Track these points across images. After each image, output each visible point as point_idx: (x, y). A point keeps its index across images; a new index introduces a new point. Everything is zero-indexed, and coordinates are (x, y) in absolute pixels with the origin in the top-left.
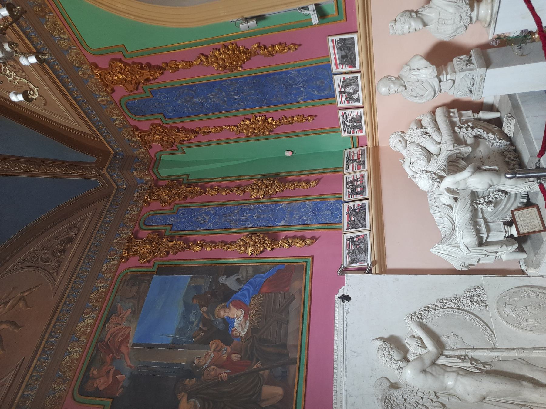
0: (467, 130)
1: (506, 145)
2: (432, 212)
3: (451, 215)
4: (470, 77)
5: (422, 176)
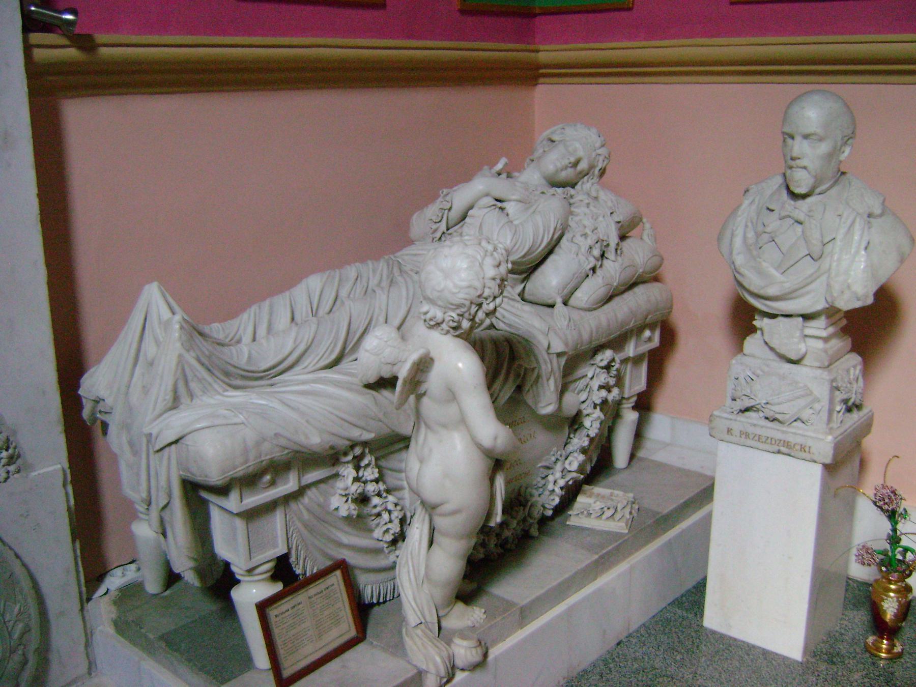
0: (601, 387)
1: (544, 508)
2: (314, 282)
3: (310, 361)
4: (805, 415)
5: (489, 262)
